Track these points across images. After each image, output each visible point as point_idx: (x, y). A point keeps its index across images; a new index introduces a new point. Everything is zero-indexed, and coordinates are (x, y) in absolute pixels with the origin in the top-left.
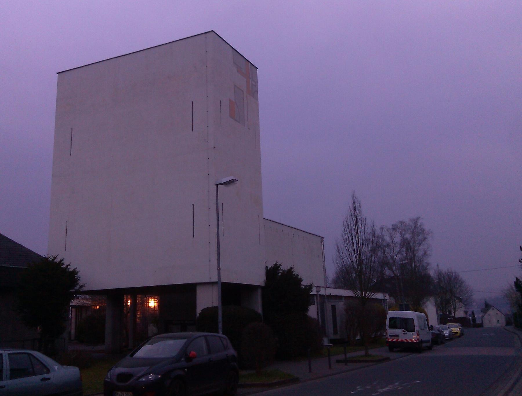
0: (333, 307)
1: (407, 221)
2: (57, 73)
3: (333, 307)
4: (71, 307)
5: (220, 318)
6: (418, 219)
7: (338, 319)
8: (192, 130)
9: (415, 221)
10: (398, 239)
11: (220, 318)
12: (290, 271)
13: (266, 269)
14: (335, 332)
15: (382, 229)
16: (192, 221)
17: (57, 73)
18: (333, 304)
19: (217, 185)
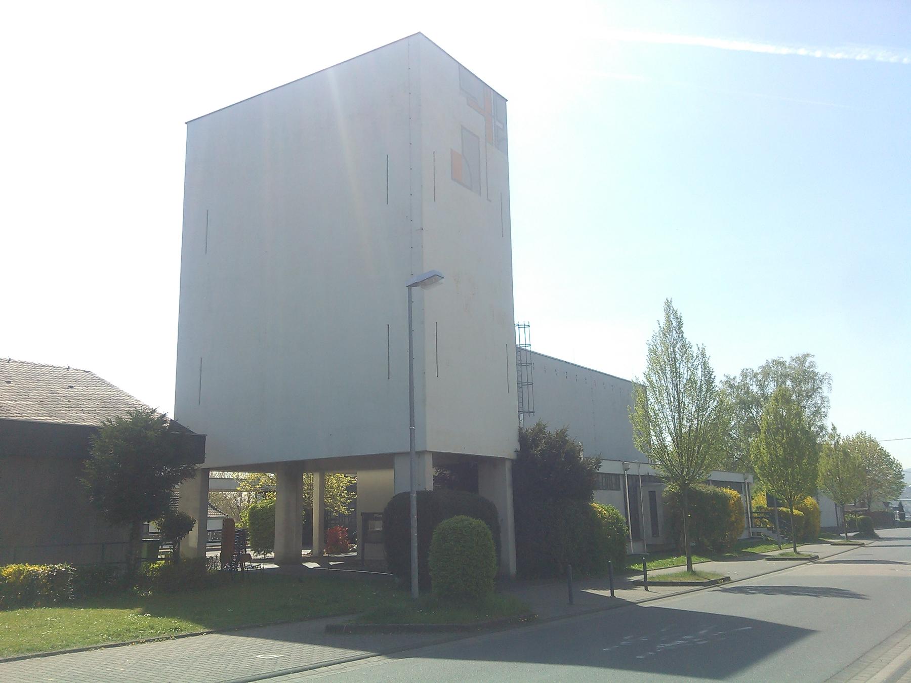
0: (652, 494)
1: (787, 359)
2: (407, 287)
3: (652, 494)
4: (356, 554)
5: (414, 511)
6: (806, 356)
7: (660, 512)
8: (386, 203)
9: (801, 360)
10: (771, 388)
11: (414, 511)
12: (562, 435)
13: (519, 432)
14: (655, 533)
15: (744, 375)
16: (388, 364)
17: (407, 287)
18: (652, 490)
19: (410, 287)
